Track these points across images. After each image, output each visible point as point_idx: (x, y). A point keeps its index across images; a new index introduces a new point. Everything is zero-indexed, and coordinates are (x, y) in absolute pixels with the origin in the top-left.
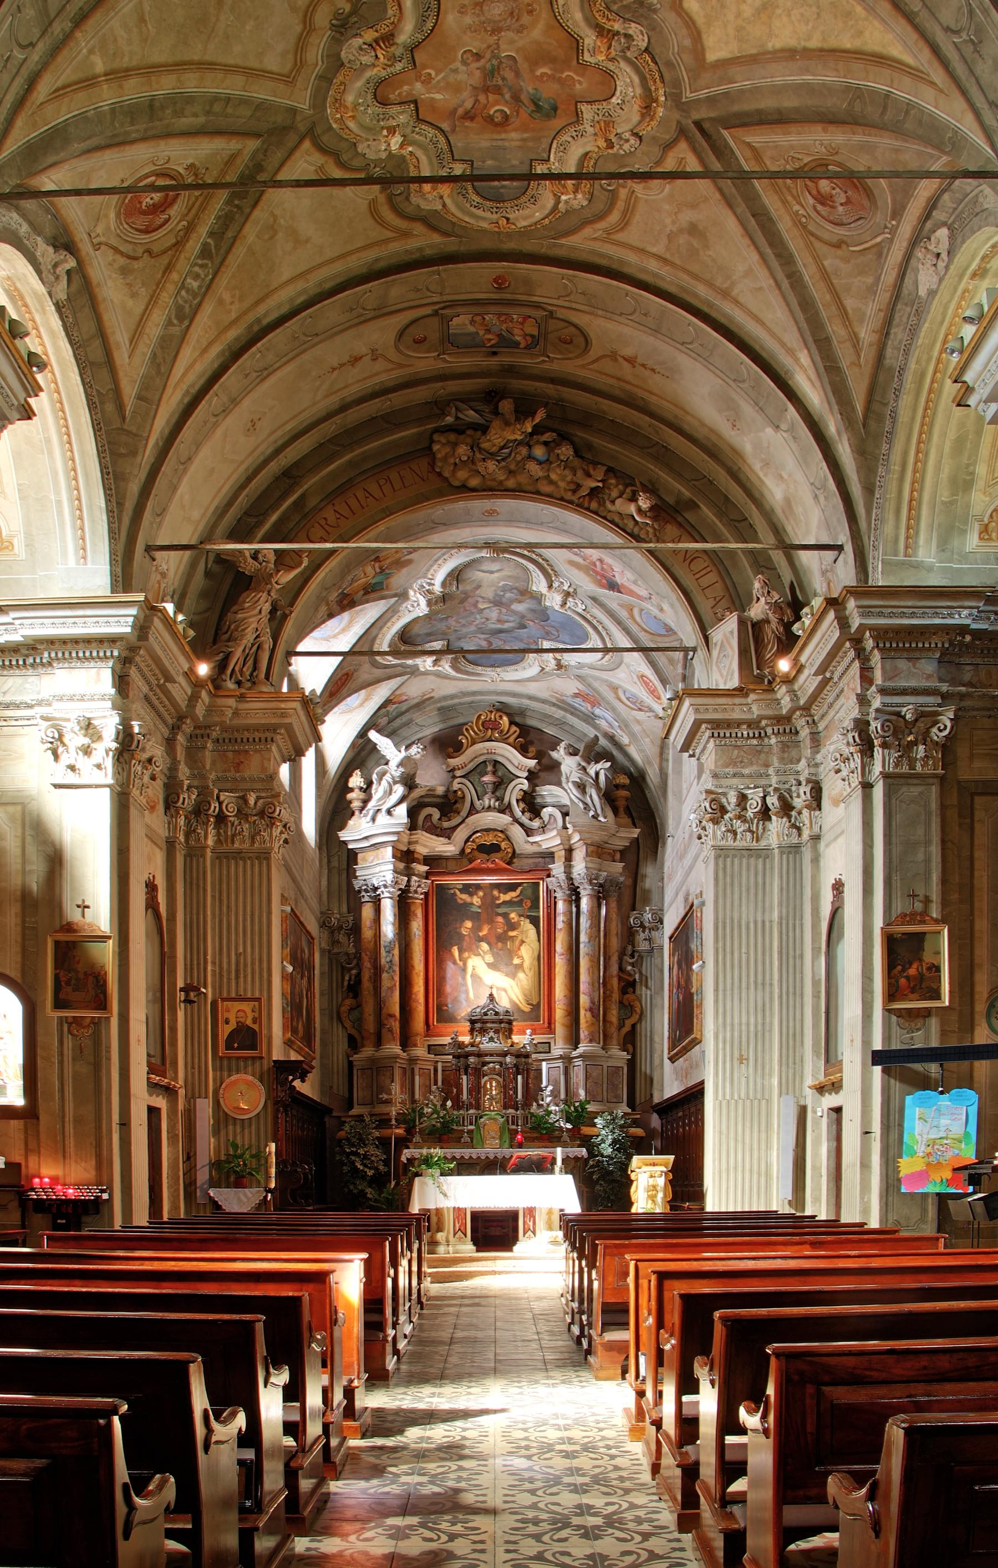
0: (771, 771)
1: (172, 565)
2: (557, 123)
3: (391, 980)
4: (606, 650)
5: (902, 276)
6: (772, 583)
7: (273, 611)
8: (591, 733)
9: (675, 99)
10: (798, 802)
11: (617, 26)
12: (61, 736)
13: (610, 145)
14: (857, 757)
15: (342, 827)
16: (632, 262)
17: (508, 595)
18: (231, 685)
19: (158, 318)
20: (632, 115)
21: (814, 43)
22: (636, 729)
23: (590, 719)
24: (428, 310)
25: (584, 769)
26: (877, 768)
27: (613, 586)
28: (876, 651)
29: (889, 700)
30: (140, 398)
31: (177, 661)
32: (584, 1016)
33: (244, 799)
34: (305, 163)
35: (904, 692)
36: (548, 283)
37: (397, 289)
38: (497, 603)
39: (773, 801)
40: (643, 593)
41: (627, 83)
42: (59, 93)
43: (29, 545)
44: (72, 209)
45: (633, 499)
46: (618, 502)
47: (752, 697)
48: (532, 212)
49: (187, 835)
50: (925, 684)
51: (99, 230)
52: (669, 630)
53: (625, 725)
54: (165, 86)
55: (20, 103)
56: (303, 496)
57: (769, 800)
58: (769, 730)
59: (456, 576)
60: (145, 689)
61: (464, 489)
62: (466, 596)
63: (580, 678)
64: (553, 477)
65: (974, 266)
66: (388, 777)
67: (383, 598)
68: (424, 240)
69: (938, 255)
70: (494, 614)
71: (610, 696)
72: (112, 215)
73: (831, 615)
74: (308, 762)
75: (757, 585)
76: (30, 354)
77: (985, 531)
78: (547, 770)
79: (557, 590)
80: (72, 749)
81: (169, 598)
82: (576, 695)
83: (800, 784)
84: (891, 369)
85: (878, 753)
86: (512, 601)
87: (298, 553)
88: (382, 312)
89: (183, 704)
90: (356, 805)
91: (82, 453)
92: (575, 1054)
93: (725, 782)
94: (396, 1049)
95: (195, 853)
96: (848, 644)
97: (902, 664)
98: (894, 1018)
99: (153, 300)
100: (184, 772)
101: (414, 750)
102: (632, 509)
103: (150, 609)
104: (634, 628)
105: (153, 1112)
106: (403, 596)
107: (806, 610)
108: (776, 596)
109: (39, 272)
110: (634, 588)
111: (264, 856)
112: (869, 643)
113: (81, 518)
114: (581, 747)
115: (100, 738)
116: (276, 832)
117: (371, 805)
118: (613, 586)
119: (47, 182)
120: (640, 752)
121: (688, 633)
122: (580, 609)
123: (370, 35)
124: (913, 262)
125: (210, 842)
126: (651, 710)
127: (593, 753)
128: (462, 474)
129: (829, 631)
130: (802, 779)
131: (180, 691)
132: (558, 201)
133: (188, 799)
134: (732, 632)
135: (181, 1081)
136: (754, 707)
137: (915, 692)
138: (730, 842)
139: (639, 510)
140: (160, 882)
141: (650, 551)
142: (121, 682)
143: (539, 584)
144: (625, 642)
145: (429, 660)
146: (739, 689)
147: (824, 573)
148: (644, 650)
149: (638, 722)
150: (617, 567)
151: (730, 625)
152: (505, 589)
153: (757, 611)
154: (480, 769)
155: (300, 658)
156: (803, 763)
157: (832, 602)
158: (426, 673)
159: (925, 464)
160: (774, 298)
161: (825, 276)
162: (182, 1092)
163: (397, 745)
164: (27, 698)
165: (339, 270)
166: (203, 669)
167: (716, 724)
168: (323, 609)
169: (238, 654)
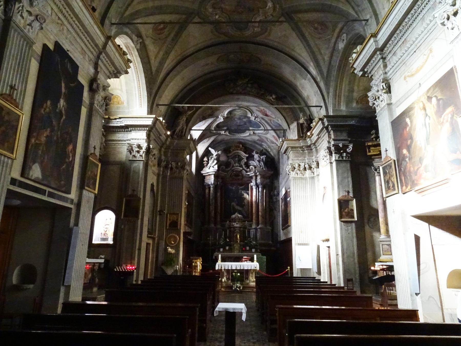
0: (306, 159)
1: (163, 109)
3: (212, 208)
4: (265, 130)
5: (335, 45)
8: (262, 149)
10: (313, 166)
12: (132, 148)
13: (266, 18)
14: (328, 156)
15: (202, 170)
16: (271, 43)
18: (175, 137)
19: (161, 53)
20: (271, 11)
22: (272, 148)
23: (261, 145)
25: (260, 157)
26: (333, 158)
27: (266, 115)
29: (336, 142)
30: (156, 71)
31: (163, 131)
32: (260, 218)
33: (177, 164)
34: (196, 20)
35: (339, 140)
36: (251, 47)
38: (240, 119)
39: (307, 166)
40: (274, 117)
43: (128, 103)
44: (142, 28)
45: (272, 96)
47: (301, 141)
48: (248, 33)
49: (163, 172)
50: (344, 138)
52: (280, 125)
53: (269, 147)
57: (306, 166)
58: (305, 149)
59: (230, 113)
60: (154, 138)
61: (232, 93)
62: (232, 117)
63: (258, 136)
65: (353, 42)
66: (213, 158)
67: (213, 117)
68: (223, 38)
69: (344, 40)
70: (239, 121)
71: (266, 140)
72: (151, 31)
73: (320, 122)
74: (194, 155)
76: (128, 59)
77: (357, 102)
78: (251, 157)
79: (254, 116)
80: (135, 151)
82: (258, 140)
83: (313, 162)
84: (333, 66)
85: (334, 155)
89: (164, 141)
90: (205, 165)
92: (258, 227)
93: (294, 161)
94: (212, 225)
95: (164, 177)
97: (339, 134)
98: (342, 223)
100: (163, 158)
101: (219, 152)
102: (271, 98)
103: (156, 120)
104: (272, 125)
105: (148, 244)
106: (218, 117)
108: (305, 118)
111: (182, 178)
112: (330, 129)
114: (259, 152)
115: (142, 148)
116: (185, 172)
117: (209, 165)
118: (266, 115)
120: (273, 153)
121: (285, 126)
122: (259, 120)
124: (338, 42)
125: (168, 174)
126: (275, 143)
127: (261, 153)
128: (231, 90)
129: (320, 126)
130: (314, 161)
131: (163, 138)
132: (254, 30)
133: (163, 164)
135: (157, 235)
136: (301, 143)
137: (342, 140)
138: (296, 176)
139: (273, 98)
140: (155, 184)
141: (276, 107)
142: (148, 136)
143: (249, 115)
145: (223, 132)
146: (298, 139)
147: (317, 112)
148: (274, 130)
149: (273, 146)
151: (295, 124)
152: (241, 116)
153: (301, 121)
154: (235, 157)
156: (314, 157)
157: (320, 119)
160: (304, 50)
162: (156, 239)
163: (216, 152)
164: (125, 139)
166: (169, 133)
167: (292, 148)
169: (178, 130)
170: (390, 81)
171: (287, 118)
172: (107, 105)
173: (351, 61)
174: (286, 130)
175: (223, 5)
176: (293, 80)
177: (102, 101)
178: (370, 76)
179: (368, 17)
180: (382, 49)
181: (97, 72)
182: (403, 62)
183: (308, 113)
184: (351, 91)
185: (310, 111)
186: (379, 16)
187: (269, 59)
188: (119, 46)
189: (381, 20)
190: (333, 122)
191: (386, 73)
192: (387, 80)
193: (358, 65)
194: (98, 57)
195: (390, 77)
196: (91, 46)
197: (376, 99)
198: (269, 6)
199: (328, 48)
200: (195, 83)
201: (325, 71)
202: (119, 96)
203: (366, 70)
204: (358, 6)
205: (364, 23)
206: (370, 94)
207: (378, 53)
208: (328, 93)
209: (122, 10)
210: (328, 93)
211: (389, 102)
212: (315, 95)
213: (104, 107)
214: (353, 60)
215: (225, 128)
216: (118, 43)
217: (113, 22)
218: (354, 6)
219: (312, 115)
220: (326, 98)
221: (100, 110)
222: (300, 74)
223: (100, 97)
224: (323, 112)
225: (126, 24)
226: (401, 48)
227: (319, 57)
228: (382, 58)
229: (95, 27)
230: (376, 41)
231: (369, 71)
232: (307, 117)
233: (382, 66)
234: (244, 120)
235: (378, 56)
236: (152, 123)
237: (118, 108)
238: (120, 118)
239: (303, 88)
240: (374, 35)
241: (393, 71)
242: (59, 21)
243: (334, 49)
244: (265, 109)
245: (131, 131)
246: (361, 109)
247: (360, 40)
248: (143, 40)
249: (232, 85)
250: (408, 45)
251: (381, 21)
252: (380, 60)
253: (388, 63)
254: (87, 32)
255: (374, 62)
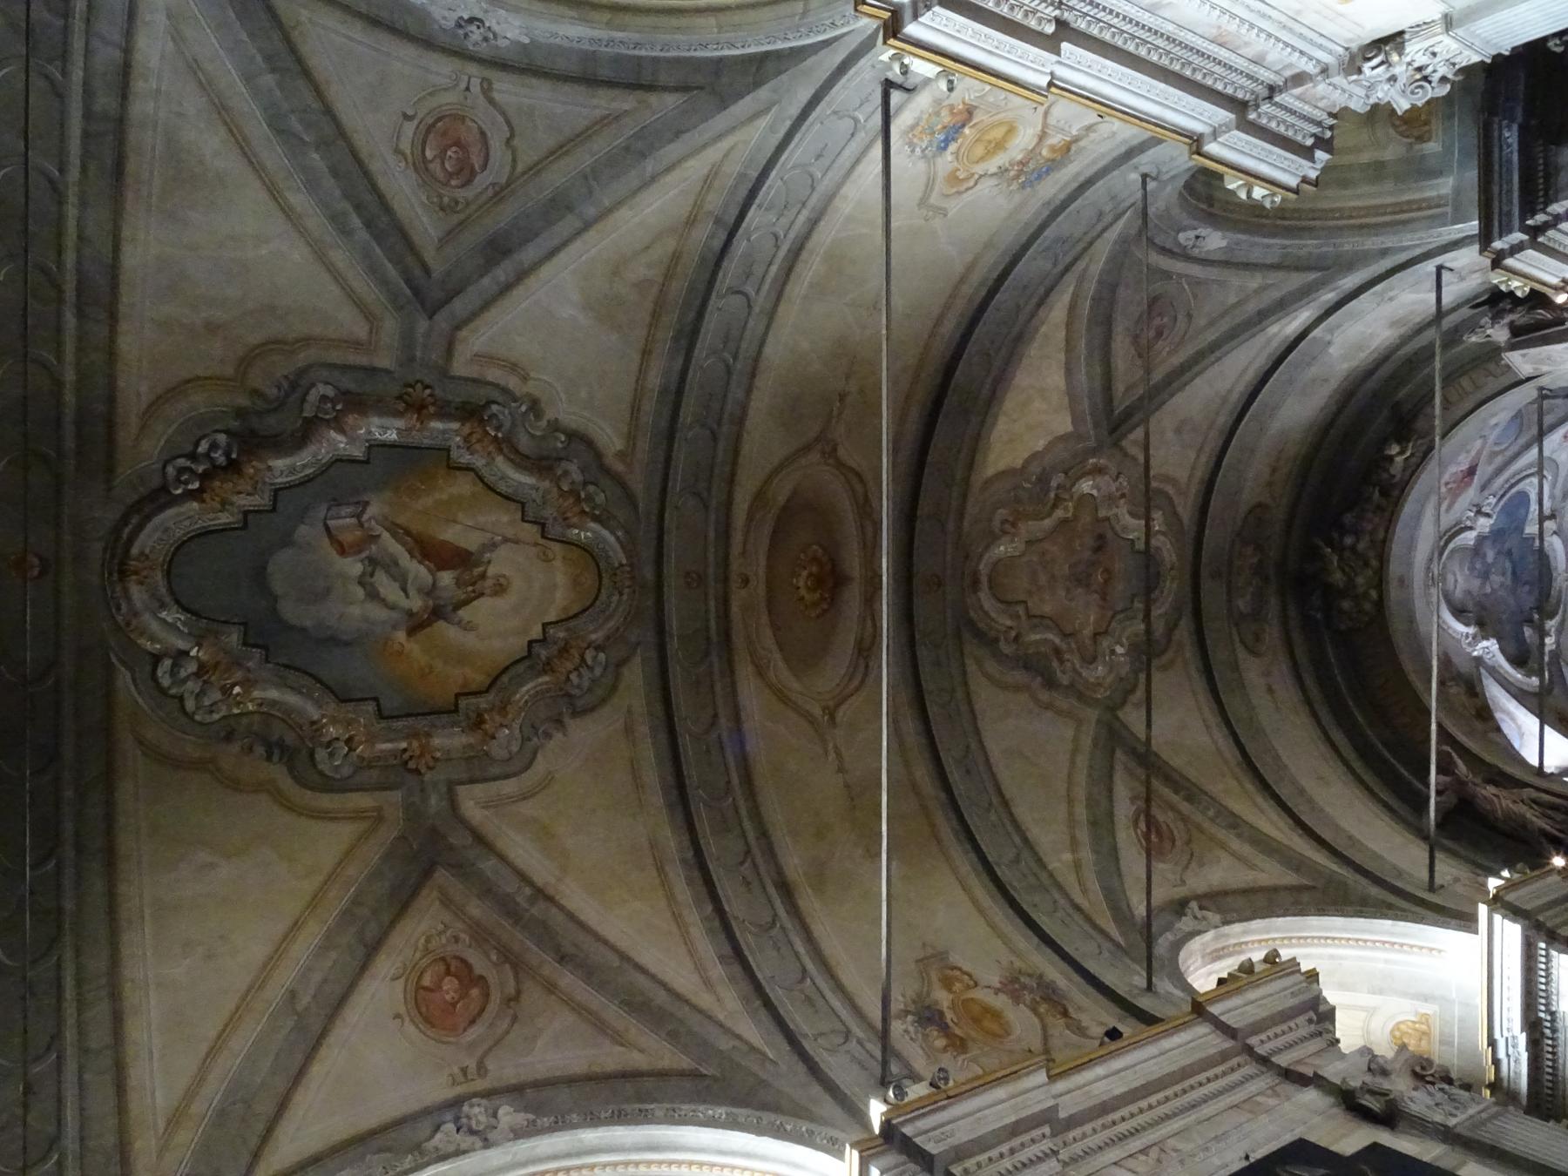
1: (1447, 870)
2: (1110, 535)
6: (1471, 326)
7: (1496, 784)
9: (1094, 452)
11: (1052, 495)
13: (1123, 496)
16: (1201, 473)
17: (1478, 566)
19: (1236, 844)
21: (1062, 356)
24: (1234, 631)
27: (1471, 472)
28: (1549, 209)
36: (1214, 537)
37: (1219, 656)
38: (1485, 576)
40: (1479, 443)
41: (1086, 486)
42: (1085, 891)
43: (1426, 998)
44: (1160, 895)
45: (1391, 459)
46: (1393, 471)
51: (1170, 876)
52: (1518, 415)
54: (1081, 812)
55: (1088, 919)
56: (1385, 744)
59: (1459, 613)
61: (1380, 604)
62: (1481, 606)
64: (1370, 527)
65: (1204, 206)
68: (1184, 632)
70: (1496, 579)
73: (1509, 262)
75: (1474, 339)
76: (1266, 960)
77: (1421, 139)
79: (1474, 520)
81: (1480, 879)
86: (1484, 563)
87: (1439, 753)
88: (1235, 667)
91: (1345, 930)
96: (1540, 239)
99: (1223, 846)
102: (1399, 459)
103: (1498, 902)
104: (1515, 448)
106: (1479, 661)
107: (1503, 288)
108: (1486, 320)
109: (1199, 933)
110: (1473, 453)
112: (1540, 218)
113: (1402, 945)
118: (1471, 472)
119: (1140, 911)
121: (1527, 393)
122: (1492, 500)
123: (1055, 664)
124: (1203, 256)
128: (1367, 606)
134: (1524, 356)
139: (1402, 453)
141: (1444, 436)
143: (1469, 538)
144: (1535, 451)
145: (1548, 641)
147: (1462, 279)
150: (1453, 469)
152: (1472, 569)
153: (1500, 334)
155: (1546, 763)
157: (1497, 263)
158: (1558, 643)
159: (1360, 208)
161: (1212, 323)
165: (1204, 696)
168: (1493, 736)
169: (1542, 823)
170: (1354, 46)
171: (1488, 391)
172: (1450, 1081)
173: (1278, 199)
174: (1541, 389)
175: (1088, 632)
176: (1334, 384)
177: (1430, 1094)
178: (1332, 122)
179: (1135, 177)
180: (1238, 106)
181: (1317, 1081)
182: (1291, 24)
183: (1466, 312)
184: (1377, 171)
185: (1454, 310)
186: (1135, 142)
187: (1254, 476)
188: (1221, 982)
189: (1148, 134)
190: (1509, 214)
191: (1325, 71)
192: (1352, 58)
193: (1288, 170)
194: (1264, 1061)
195: (1341, 50)
196: (1224, 1074)
197: (1425, 78)
198: (1093, 487)
199: (1222, 284)
200: (1338, 736)
201: (1297, 280)
202: (1397, 1027)
203: (1309, 142)
204: (1101, 214)
205: (1151, 185)
206: (1402, 105)
207: (1252, 116)
208: (1384, 253)
209: (1107, 945)
210: (1384, 253)
211: (1439, 29)
212: (1391, 299)
213: (1455, 1090)
214: (1274, 194)
215: (1528, 632)
216: (1212, 985)
217: (1144, 984)
218: (1099, 227)
219: (1476, 297)
220: (1403, 257)
221: (1471, 1111)
222: (1309, 364)
223: (1414, 1094)
224: (1468, 258)
225: (1150, 943)
226: (1239, 47)
227: (1252, 307)
228: (1270, 98)
229: (1166, 1044)
230: (1215, 134)
231: (1315, 130)
232: (1484, 314)
233: (1297, 91)
234: (1490, 556)
235: (1265, 114)
236: (1514, 921)
237: (1445, 1041)
238: (1492, 1043)
239: (1360, 348)
240: (1196, 142)
241: (1320, 47)
242: (1154, 1153)
243: (1226, 263)
244: (1446, 477)
245: (1553, 1014)
246: (1451, 117)
247: (1204, 190)
248: (1197, 897)
249: (1346, 605)
250: (1233, 26)
251: (1149, 134)
252: (1276, 104)
253: (1288, 73)
254: (1185, 1073)
255: (1284, 122)
